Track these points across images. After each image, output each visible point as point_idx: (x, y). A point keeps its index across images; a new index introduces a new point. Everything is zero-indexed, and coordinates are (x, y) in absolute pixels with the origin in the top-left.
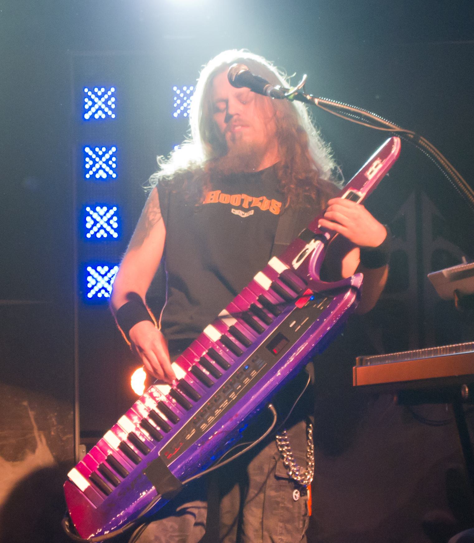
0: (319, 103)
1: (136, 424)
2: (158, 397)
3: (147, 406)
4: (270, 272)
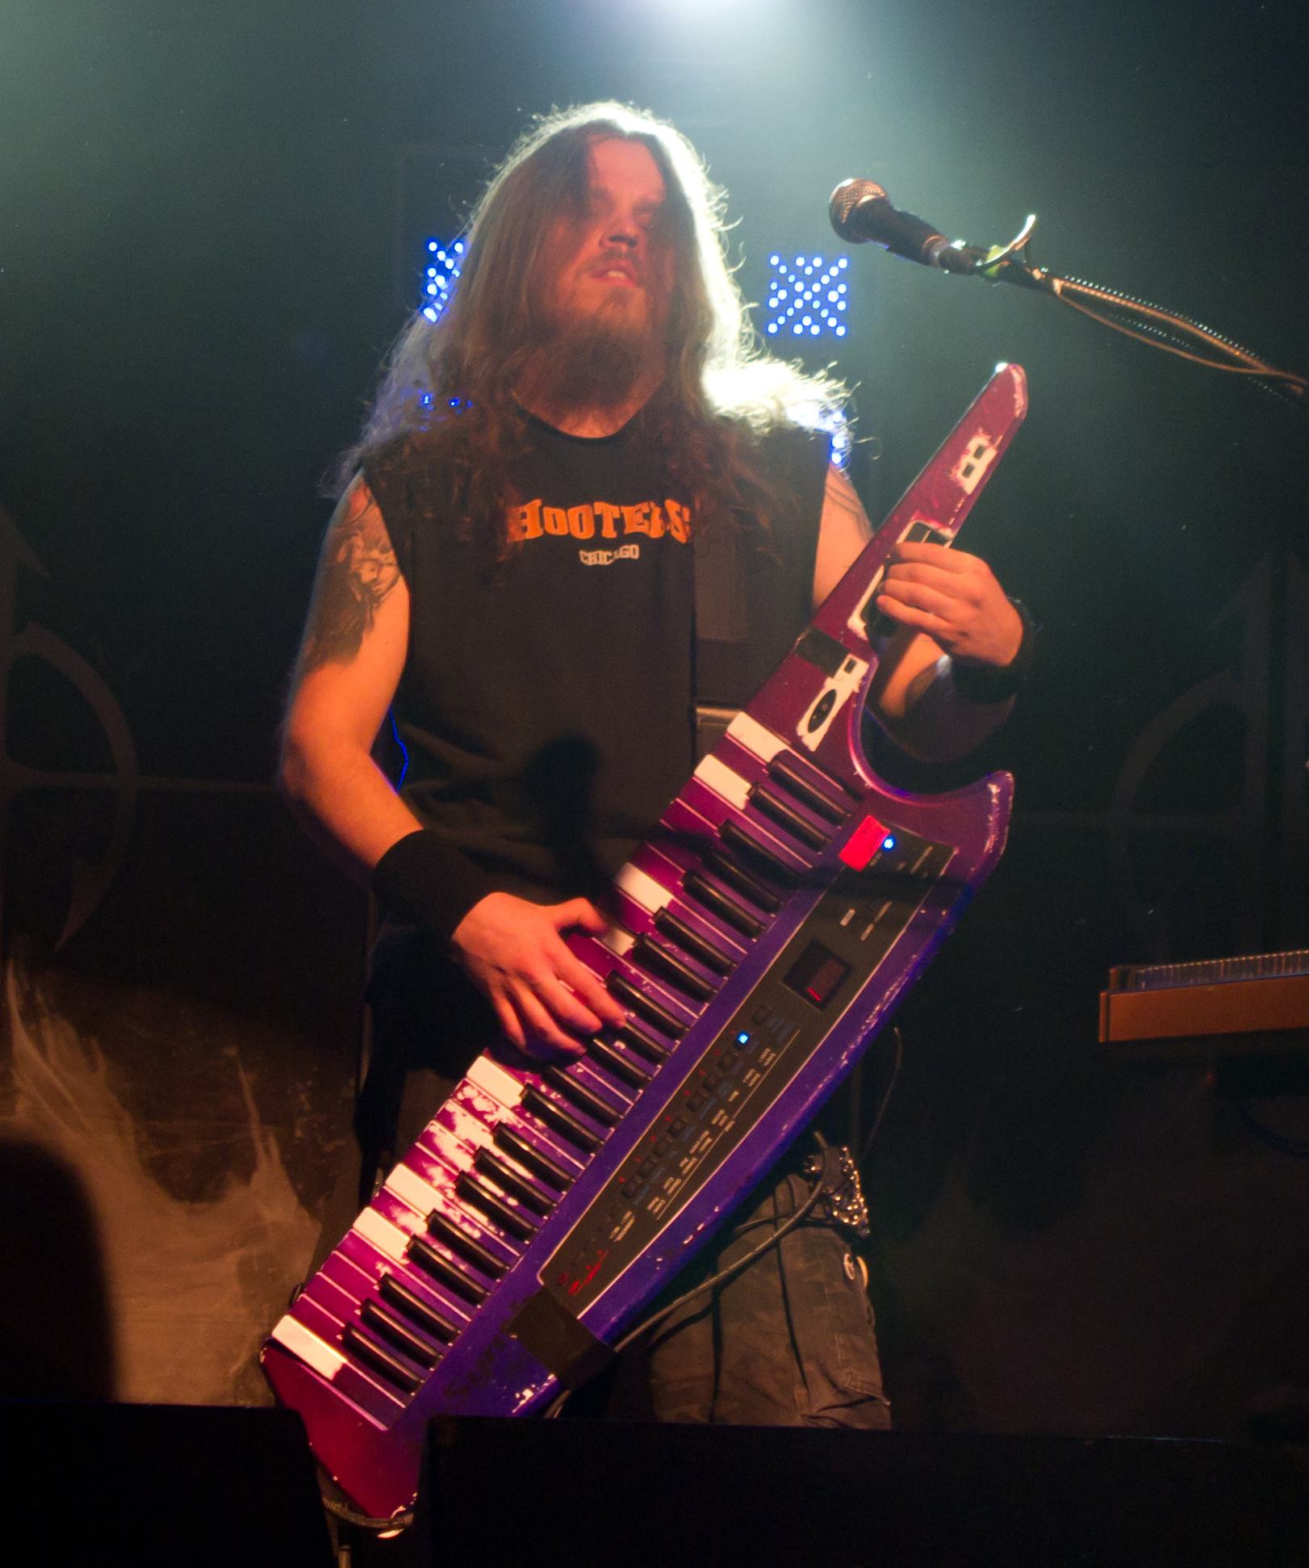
0: (1064, 290)
1: (441, 1189)
2: (491, 1113)
3: (464, 1137)
4: (738, 758)
